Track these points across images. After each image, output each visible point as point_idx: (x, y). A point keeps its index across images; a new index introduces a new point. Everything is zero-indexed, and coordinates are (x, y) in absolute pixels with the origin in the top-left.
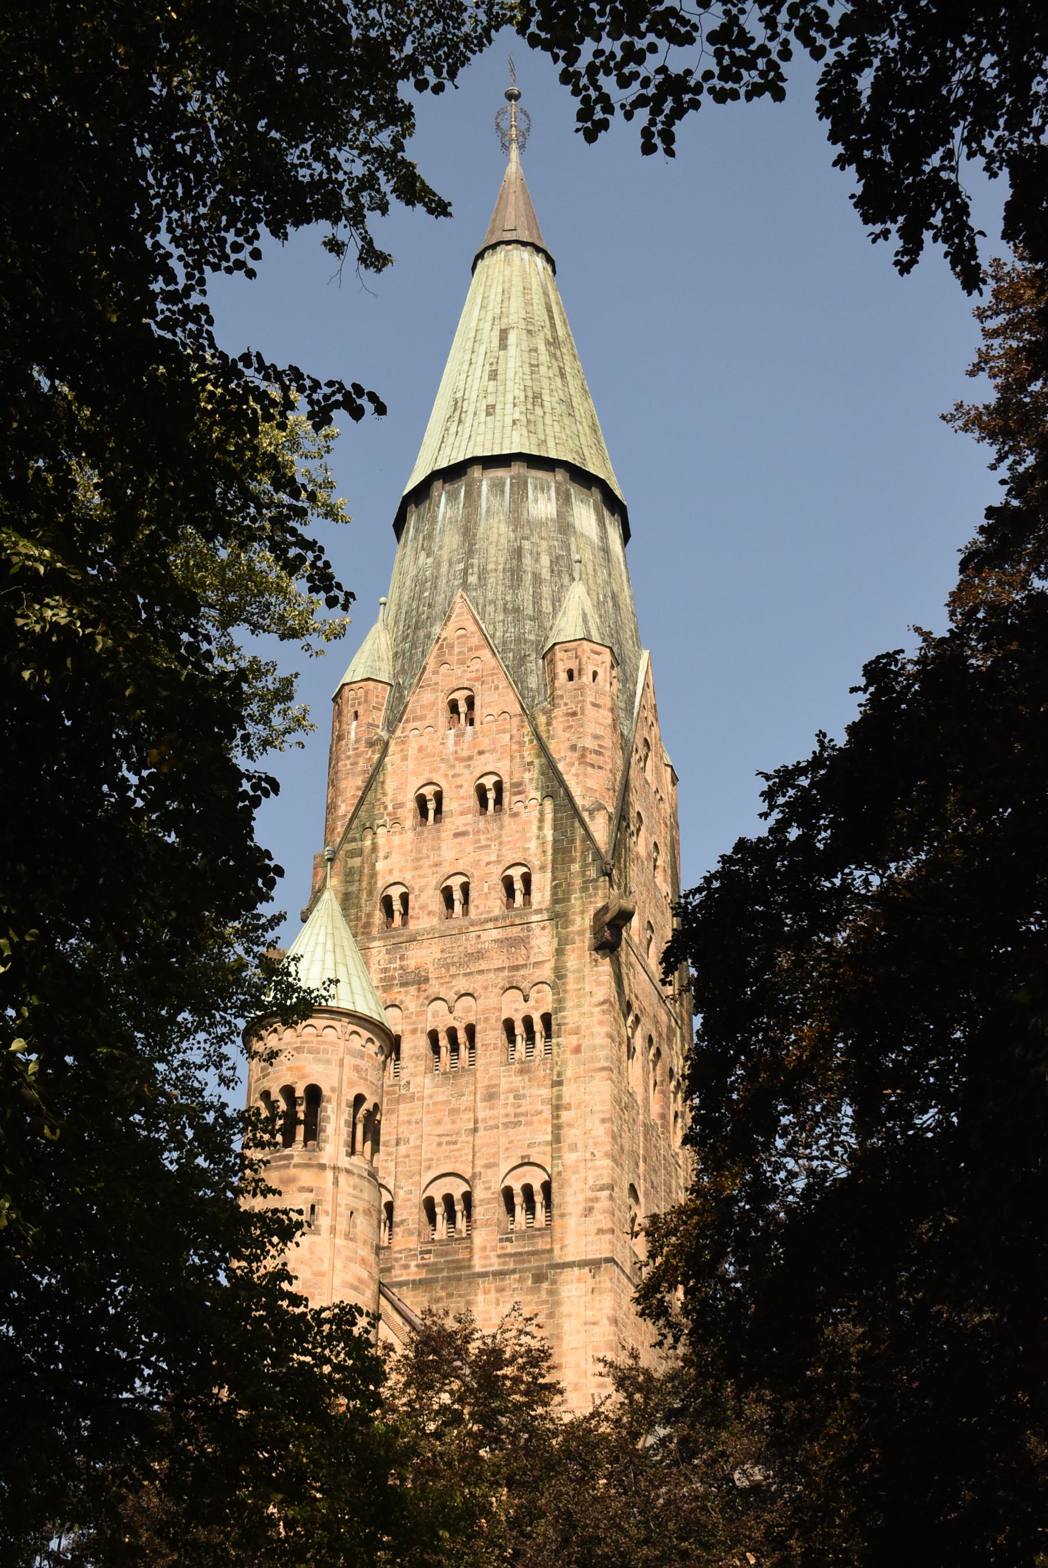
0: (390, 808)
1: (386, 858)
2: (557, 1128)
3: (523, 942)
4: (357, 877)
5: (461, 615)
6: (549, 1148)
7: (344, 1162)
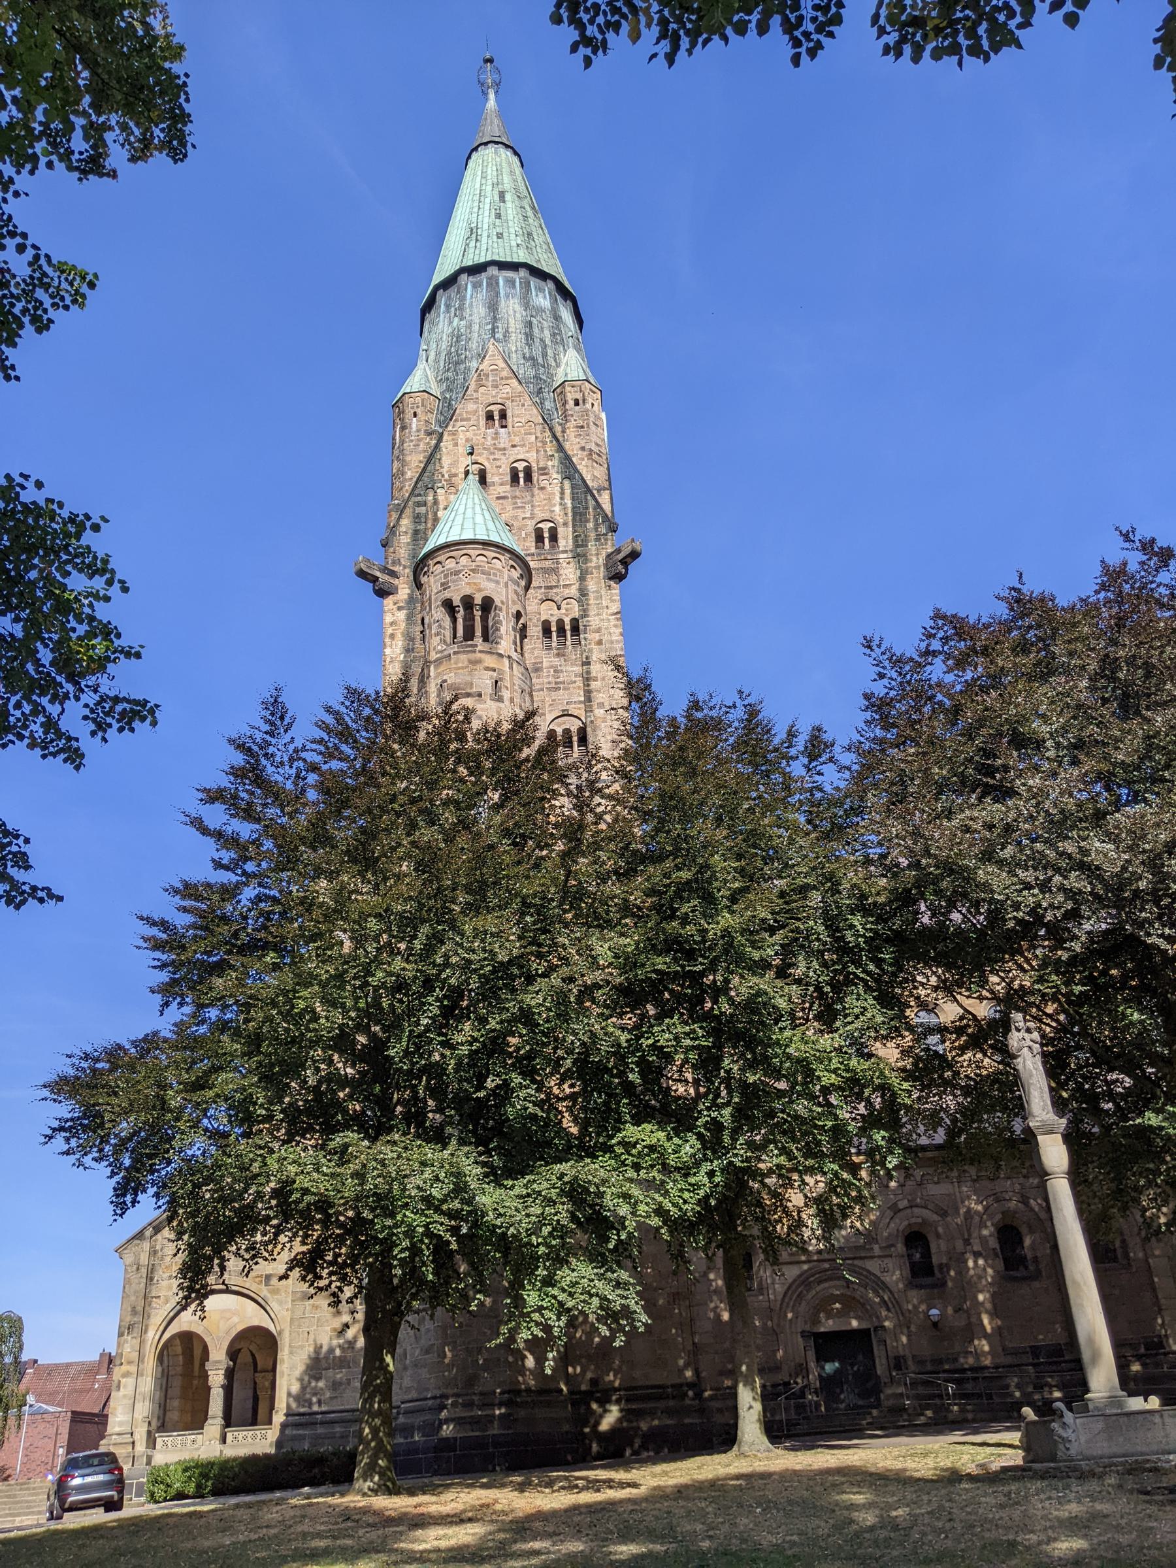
0: (446, 476)
1: (445, 509)
3: (555, 571)
4: (423, 520)
5: (493, 361)
6: (582, 706)
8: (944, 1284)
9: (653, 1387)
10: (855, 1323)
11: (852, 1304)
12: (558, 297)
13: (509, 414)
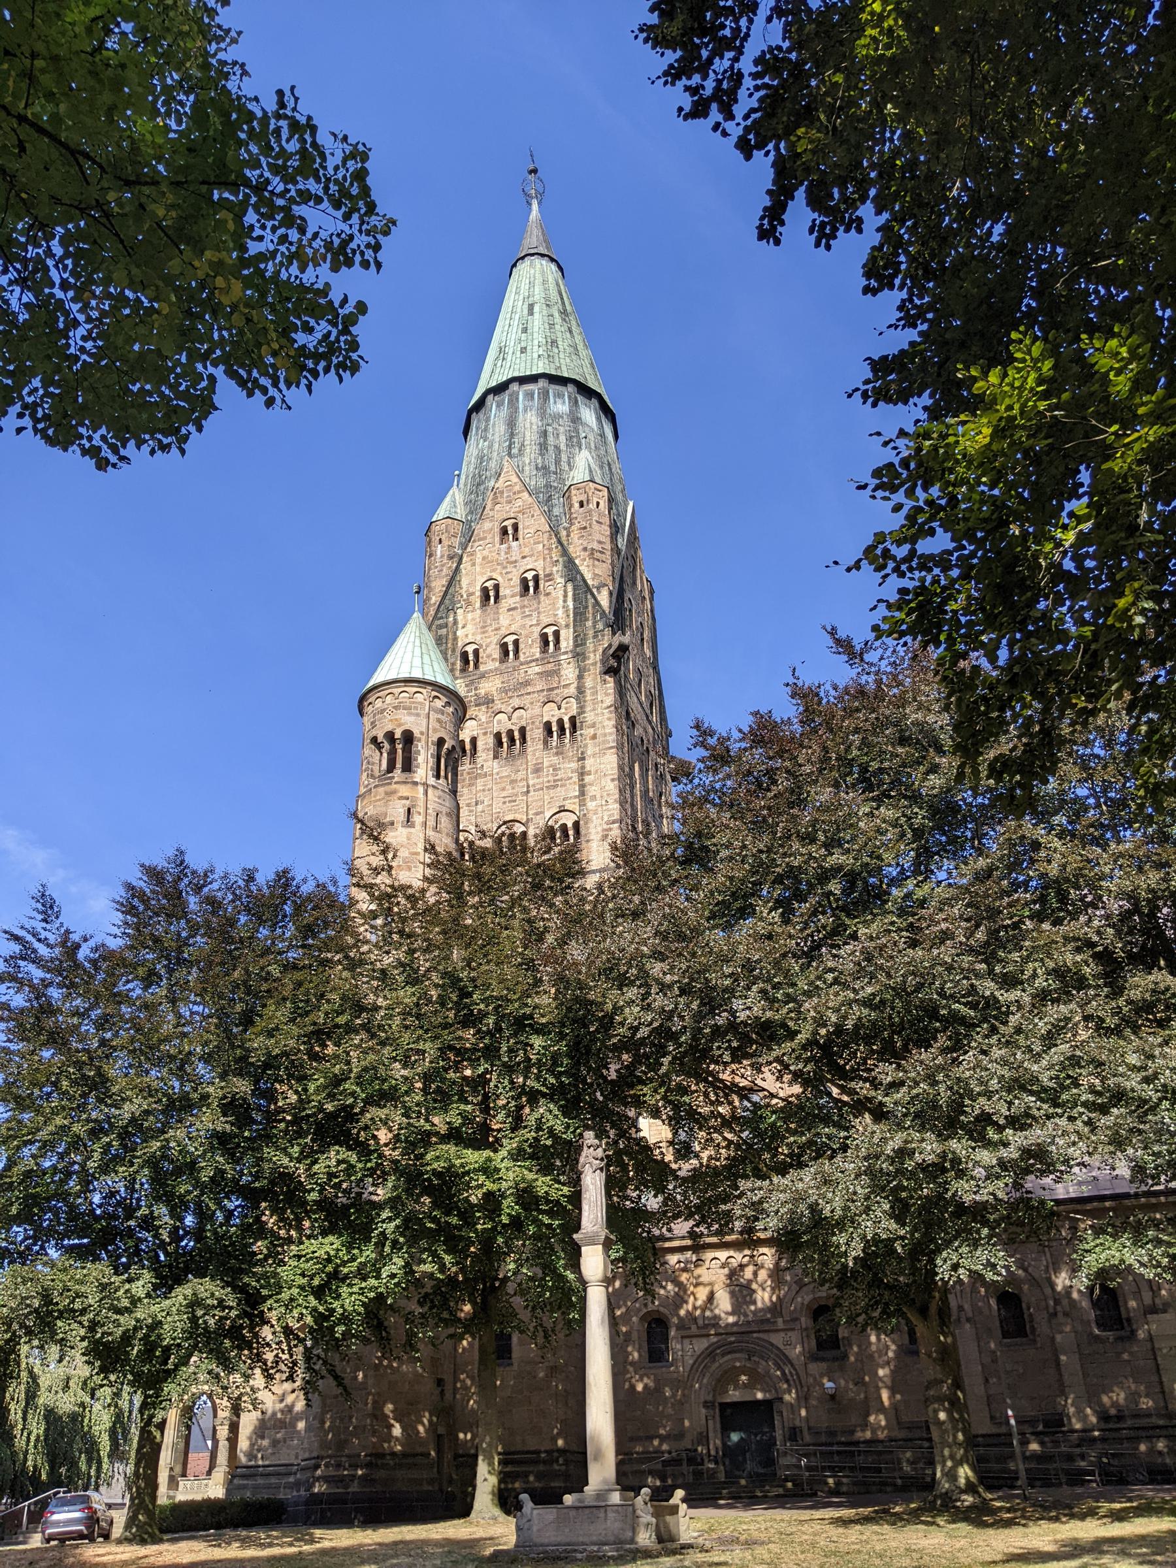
2: (582, 787)
3: (557, 672)
5: (509, 477)
7: (432, 781)
8: (845, 1357)
9: (528, 1452)
10: (760, 1396)
11: (757, 1379)
12: (579, 398)
13: (520, 526)
